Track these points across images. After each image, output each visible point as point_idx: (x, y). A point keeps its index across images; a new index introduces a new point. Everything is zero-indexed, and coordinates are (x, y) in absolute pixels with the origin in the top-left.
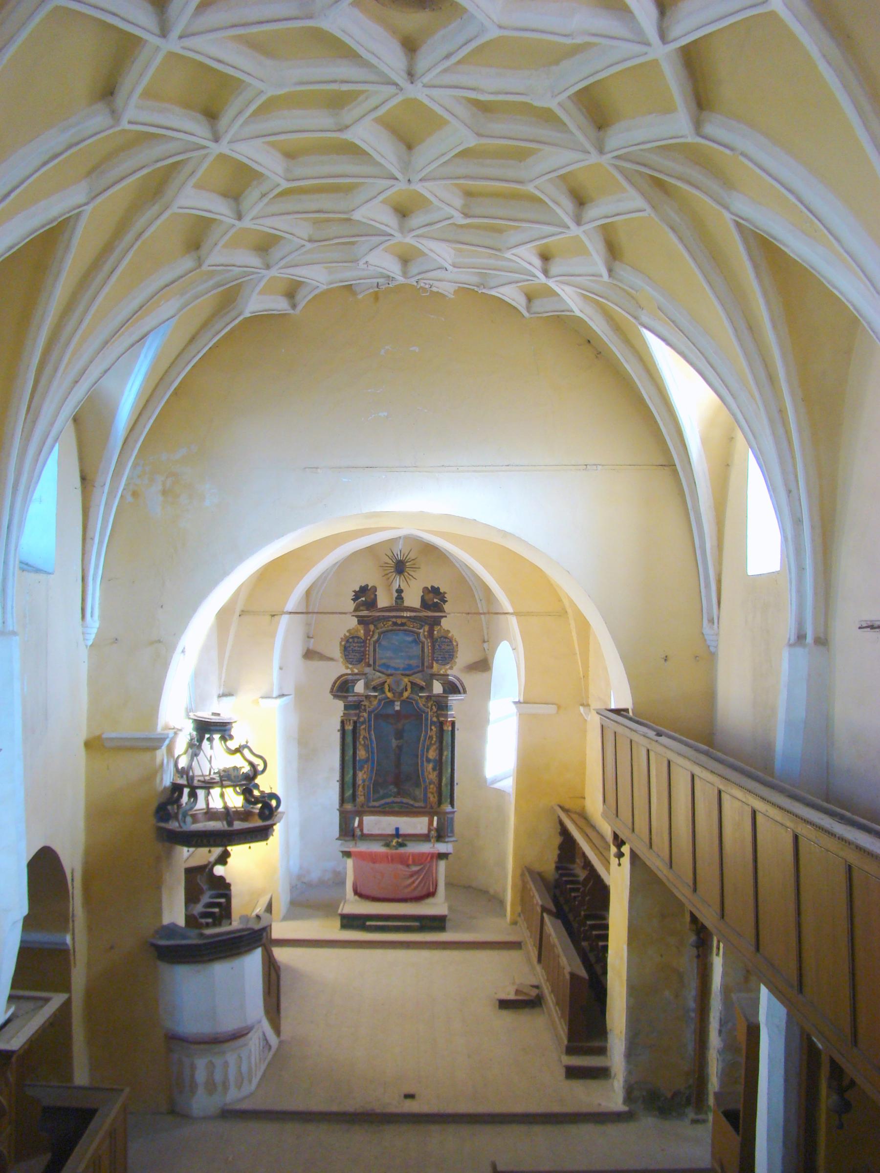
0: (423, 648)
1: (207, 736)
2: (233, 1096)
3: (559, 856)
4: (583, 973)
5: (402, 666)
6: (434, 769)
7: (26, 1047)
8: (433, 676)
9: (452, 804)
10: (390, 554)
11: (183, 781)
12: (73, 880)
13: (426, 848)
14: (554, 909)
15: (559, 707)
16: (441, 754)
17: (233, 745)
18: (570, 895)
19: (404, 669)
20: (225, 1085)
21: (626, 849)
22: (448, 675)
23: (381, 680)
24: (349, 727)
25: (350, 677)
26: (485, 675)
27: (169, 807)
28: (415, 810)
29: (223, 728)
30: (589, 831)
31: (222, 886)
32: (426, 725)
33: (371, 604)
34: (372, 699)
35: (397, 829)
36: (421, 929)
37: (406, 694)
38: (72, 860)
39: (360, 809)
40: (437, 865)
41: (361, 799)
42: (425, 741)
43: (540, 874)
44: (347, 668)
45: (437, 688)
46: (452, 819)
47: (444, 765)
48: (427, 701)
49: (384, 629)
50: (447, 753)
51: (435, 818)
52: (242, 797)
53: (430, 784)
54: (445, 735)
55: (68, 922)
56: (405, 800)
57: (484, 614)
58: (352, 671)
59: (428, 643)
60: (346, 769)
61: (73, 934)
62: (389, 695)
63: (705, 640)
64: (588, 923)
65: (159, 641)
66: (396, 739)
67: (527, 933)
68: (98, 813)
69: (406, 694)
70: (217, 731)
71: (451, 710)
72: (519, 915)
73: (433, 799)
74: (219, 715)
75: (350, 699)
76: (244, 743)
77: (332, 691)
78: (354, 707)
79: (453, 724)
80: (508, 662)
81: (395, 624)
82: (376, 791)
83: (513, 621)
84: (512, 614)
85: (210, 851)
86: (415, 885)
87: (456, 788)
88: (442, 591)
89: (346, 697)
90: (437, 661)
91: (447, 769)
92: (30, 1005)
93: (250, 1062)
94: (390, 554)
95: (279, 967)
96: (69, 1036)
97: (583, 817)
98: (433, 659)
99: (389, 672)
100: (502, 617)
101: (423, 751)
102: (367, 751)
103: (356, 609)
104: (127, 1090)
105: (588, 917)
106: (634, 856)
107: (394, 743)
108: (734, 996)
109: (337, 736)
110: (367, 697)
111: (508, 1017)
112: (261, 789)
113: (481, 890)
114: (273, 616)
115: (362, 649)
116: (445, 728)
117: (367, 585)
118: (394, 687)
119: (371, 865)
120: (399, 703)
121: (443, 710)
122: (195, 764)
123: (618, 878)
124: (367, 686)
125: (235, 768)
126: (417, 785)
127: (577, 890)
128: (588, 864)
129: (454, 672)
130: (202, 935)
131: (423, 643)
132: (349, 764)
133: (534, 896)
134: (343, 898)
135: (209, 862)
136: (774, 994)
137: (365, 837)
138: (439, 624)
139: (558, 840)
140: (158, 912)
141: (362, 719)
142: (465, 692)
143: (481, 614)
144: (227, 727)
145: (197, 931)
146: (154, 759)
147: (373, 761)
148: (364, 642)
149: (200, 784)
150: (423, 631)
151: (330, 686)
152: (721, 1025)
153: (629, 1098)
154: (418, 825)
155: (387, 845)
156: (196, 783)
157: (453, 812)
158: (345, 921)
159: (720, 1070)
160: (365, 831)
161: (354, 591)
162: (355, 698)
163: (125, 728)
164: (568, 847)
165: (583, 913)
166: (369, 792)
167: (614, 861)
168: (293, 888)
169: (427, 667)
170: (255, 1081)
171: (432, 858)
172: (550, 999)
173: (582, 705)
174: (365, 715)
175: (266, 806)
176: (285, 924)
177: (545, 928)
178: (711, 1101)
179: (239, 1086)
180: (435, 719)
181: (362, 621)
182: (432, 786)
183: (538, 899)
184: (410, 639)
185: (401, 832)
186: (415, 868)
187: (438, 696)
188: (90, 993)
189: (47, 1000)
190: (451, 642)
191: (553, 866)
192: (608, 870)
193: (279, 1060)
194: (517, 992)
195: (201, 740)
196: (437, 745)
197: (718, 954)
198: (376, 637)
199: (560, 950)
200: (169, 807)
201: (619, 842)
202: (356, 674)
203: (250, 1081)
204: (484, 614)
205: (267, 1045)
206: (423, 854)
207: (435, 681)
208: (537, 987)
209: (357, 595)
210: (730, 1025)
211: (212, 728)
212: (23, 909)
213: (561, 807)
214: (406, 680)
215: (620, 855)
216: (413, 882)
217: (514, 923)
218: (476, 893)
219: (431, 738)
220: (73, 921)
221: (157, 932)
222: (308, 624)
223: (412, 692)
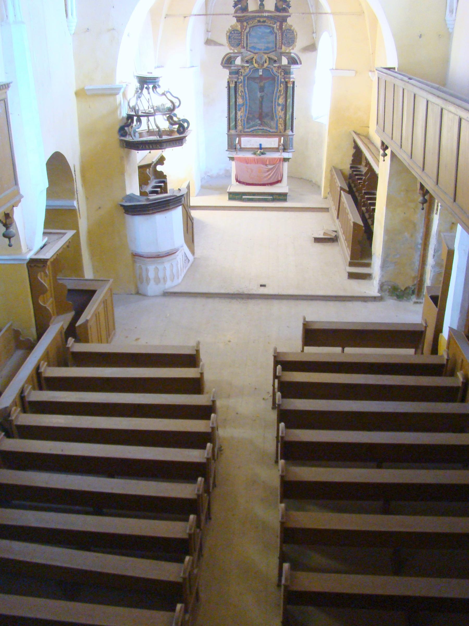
0: (276, 37)
1: (145, 86)
2: (169, 285)
4: (361, 223)
5: (263, 48)
6: (282, 110)
7: (55, 257)
8: (282, 54)
9: (292, 130)
11: (133, 113)
12: (75, 171)
13: (277, 155)
14: (347, 189)
15: (356, 72)
16: (286, 101)
17: (160, 90)
18: (358, 184)
19: (265, 50)
20: (165, 279)
21: (388, 152)
22: (291, 53)
23: (251, 56)
24: (232, 85)
25: (232, 55)
26: (314, 53)
27: (126, 128)
28: (271, 133)
29: (154, 81)
30: (371, 146)
31: (161, 177)
32: (278, 84)
33: (245, 9)
34: (246, 68)
35: (261, 145)
36: (273, 200)
37: (266, 65)
38: (74, 160)
39: (239, 133)
40: (283, 164)
41: (240, 128)
43: (341, 171)
44: (231, 49)
45: (285, 61)
46: (292, 139)
47: (288, 107)
48: (278, 70)
49: (252, 25)
50: (289, 100)
51: (282, 138)
52: (168, 122)
53: (279, 118)
54: (288, 89)
55: (74, 195)
56: (265, 128)
57: (313, 13)
58: (234, 51)
59: (279, 33)
60: (231, 110)
61: (78, 201)
62: (256, 65)
63: (446, 25)
64: (366, 196)
65: (114, 29)
66: (260, 92)
67: (332, 203)
68: (86, 134)
69: (266, 65)
70: (151, 83)
72: (329, 193)
73: (281, 127)
74: (151, 73)
75: (233, 68)
76: (167, 90)
77: (222, 64)
78: (235, 73)
79: (293, 83)
80: (327, 43)
81: (259, 21)
83: (330, 18)
84: (330, 14)
85: (150, 152)
86: (271, 176)
89: (231, 67)
90: (285, 44)
91: (289, 110)
92: (56, 237)
93: (177, 267)
95: (193, 218)
96: (80, 255)
97: (367, 138)
98: (282, 43)
99: (256, 51)
100: (324, 15)
101: (276, 99)
103: (236, 12)
104: (111, 280)
105: (366, 193)
106: (393, 155)
107: (259, 94)
108: (442, 234)
109: (226, 91)
110: (243, 67)
111: (319, 246)
112: (178, 117)
113: (308, 180)
114: (185, 17)
115: (240, 38)
116: (289, 85)
118: (258, 60)
119: (246, 165)
121: (287, 74)
122: (139, 102)
123: (383, 169)
124: (242, 60)
125: (163, 105)
126: (272, 119)
127: (361, 179)
128: (368, 164)
129: (295, 51)
130: (148, 200)
131: (276, 34)
132: (233, 107)
133: (337, 182)
134: (230, 184)
135: (153, 162)
136: (464, 229)
137: (242, 149)
138: (286, 21)
139: (353, 151)
140: (124, 189)
141: (240, 80)
142: (301, 63)
143: (311, 14)
144: (157, 80)
145: (145, 198)
146: (115, 100)
148: (241, 33)
149: (143, 114)
150: (276, 26)
151: (222, 59)
152: (435, 252)
153: (381, 288)
154: (272, 142)
155: (255, 154)
156: (140, 114)
157: (293, 135)
159: (431, 277)
160: (242, 146)
162: (236, 68)
163: (98, 84)
164: (358, 155)
165: (363, 191)
166: (244, 124)
167: (381, 158)
168: (202, 179)
169: (278, 48)
170: (181, 278)
172: (342, 238)
173: (371, 71)
174: (242, 78)
175: (181, 126)
176: (199, 198)
177: (342, 199)
178: (425, 291)
179: (172, 280)
180: (283, 80)
181: (239, 20)
182: (280, 120)
183: (339, 183)
184: (268, 31)
185: (263, 147)
186: (270, 167)
187: (285, 66)
188: (90, 233)
189: (64, 234)
190: (293, 32)
191: (349, 166)
192: (378, 166)
193: (194, 267)
194: (325, 234)
195: (142, 89)
196: (284, 95)
197: (436, 214)
198: (248, 30)
199: (349, 210)
200: (126, 128)
201: (385, 147)
202: (236, 53)
203: (178, 278)
204: (313, 13)
205: (187, 259)
206: (275, 159)
207: (283, 57)
208: (336, 231)
210: (440, 252)
211: (148, 81)
212: (46, 184)
213: (355, 133)
214: (266, 56)
215: (385, 155)
216: (269, 175)
217: (326, 198)
218: (305, 182)
219: (280, 91)
220: (77, 194)
221: (123, 199)
222: (207, 23)
223: (269, 64)
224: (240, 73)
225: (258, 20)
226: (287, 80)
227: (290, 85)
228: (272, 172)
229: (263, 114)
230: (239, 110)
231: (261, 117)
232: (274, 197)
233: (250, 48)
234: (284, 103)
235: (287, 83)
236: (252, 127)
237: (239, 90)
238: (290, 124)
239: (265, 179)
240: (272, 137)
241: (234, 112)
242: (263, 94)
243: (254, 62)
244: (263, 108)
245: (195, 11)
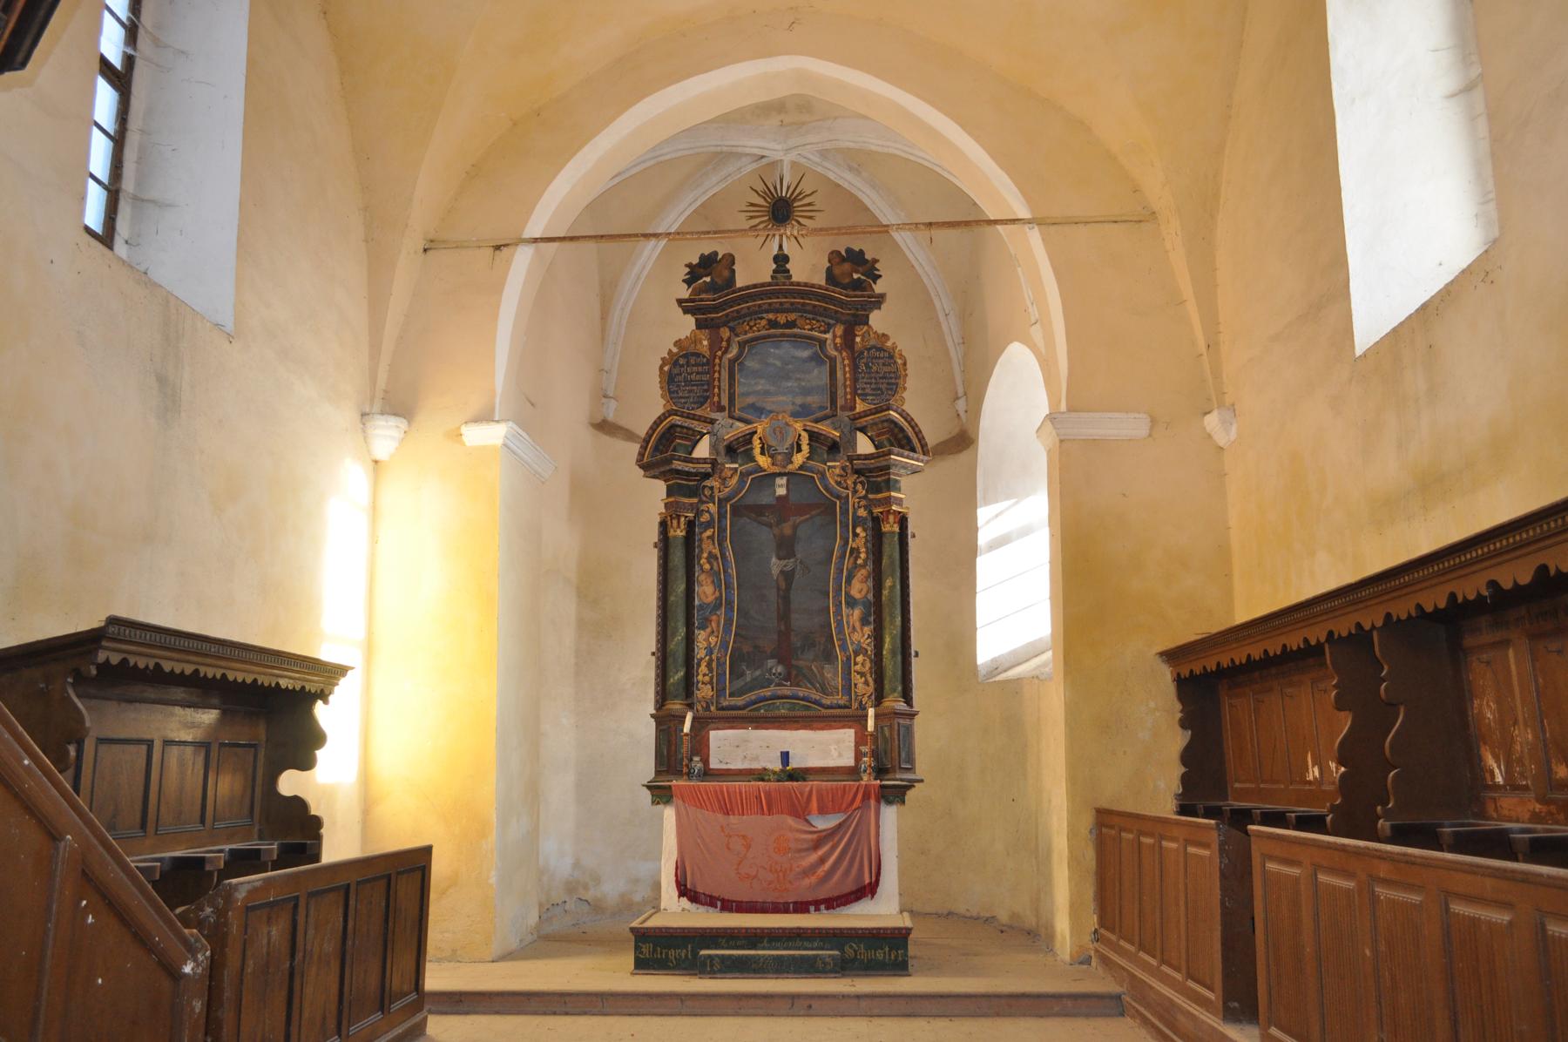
3: (1185, 779)
6: (864, 621)
9: (907, 696)
10: (760, 187)
15: (1154, 421)
24: (678, 532)
26: (964, 457)
36: (843, 968)
37: (799, 459)
41: (704, 692)
42: (842, 556)
46: (909, 730)
47: (889, 609)
53: (857, 654)
54: (888, 548)
56: (801, 692)
60: (671, 624)
62: (763, 461)
69: (799, 459)
71: (899, 490)
79: (903, 521)
80: (1019, 398)
81: (773, 324)
82: (736, 673)
83: (1034, 236)
84: (1029, 222)
87: (915, 663)
88: (868, 257)
90: (864, 397)
91: (893, 617)
94: (760, 187)
98: (855, 393)
102: (717, 586)
107: (776, 565)
114: (498, 248)
115: (706, 378)
116: (886, 528)
117: (716, 253)
118: (772, 442)
119: (720, 816)
120: (783, 481)
121: (879, 491)
124: (713, 447)
138: (865, 321)
141: (705, 517)
147: (729, 603)
154: (830, 748)
157: (912, 716)
158: (646, 949)
161: (689, 265)
166: (721, 675)
171: (866, 796)
174: (713, 508)
180: (862, 513)
182: (860, 659)
184: (806, 354)
186: (823, 823)
190: (891, 357)
196: (870, 567)
198: (734, 351)
209: (694, 274)
214: (798, 426)
216: (822, 861)
224: (707, 492)
225: (770, 321)
226: (877, 511)
227: (891, 527)
228: (833, 848)
229: (796, 641)
230: (703, 627)
231: (784, 654)
232: (849, 952)
233: (742, 409)
234: (870, 597)
235: (877, 521)
236: (751, 690)
237: (701, 551)
238: (899, 673)
239: (807, 882)
240: (831, 728)
241: (682, 631)
242: (789, 564)
243: (757, 451)
244: (794, 616)
245: (535, 229)
